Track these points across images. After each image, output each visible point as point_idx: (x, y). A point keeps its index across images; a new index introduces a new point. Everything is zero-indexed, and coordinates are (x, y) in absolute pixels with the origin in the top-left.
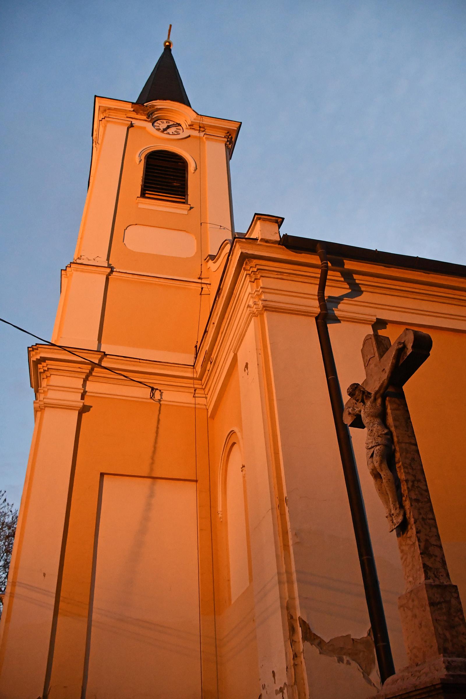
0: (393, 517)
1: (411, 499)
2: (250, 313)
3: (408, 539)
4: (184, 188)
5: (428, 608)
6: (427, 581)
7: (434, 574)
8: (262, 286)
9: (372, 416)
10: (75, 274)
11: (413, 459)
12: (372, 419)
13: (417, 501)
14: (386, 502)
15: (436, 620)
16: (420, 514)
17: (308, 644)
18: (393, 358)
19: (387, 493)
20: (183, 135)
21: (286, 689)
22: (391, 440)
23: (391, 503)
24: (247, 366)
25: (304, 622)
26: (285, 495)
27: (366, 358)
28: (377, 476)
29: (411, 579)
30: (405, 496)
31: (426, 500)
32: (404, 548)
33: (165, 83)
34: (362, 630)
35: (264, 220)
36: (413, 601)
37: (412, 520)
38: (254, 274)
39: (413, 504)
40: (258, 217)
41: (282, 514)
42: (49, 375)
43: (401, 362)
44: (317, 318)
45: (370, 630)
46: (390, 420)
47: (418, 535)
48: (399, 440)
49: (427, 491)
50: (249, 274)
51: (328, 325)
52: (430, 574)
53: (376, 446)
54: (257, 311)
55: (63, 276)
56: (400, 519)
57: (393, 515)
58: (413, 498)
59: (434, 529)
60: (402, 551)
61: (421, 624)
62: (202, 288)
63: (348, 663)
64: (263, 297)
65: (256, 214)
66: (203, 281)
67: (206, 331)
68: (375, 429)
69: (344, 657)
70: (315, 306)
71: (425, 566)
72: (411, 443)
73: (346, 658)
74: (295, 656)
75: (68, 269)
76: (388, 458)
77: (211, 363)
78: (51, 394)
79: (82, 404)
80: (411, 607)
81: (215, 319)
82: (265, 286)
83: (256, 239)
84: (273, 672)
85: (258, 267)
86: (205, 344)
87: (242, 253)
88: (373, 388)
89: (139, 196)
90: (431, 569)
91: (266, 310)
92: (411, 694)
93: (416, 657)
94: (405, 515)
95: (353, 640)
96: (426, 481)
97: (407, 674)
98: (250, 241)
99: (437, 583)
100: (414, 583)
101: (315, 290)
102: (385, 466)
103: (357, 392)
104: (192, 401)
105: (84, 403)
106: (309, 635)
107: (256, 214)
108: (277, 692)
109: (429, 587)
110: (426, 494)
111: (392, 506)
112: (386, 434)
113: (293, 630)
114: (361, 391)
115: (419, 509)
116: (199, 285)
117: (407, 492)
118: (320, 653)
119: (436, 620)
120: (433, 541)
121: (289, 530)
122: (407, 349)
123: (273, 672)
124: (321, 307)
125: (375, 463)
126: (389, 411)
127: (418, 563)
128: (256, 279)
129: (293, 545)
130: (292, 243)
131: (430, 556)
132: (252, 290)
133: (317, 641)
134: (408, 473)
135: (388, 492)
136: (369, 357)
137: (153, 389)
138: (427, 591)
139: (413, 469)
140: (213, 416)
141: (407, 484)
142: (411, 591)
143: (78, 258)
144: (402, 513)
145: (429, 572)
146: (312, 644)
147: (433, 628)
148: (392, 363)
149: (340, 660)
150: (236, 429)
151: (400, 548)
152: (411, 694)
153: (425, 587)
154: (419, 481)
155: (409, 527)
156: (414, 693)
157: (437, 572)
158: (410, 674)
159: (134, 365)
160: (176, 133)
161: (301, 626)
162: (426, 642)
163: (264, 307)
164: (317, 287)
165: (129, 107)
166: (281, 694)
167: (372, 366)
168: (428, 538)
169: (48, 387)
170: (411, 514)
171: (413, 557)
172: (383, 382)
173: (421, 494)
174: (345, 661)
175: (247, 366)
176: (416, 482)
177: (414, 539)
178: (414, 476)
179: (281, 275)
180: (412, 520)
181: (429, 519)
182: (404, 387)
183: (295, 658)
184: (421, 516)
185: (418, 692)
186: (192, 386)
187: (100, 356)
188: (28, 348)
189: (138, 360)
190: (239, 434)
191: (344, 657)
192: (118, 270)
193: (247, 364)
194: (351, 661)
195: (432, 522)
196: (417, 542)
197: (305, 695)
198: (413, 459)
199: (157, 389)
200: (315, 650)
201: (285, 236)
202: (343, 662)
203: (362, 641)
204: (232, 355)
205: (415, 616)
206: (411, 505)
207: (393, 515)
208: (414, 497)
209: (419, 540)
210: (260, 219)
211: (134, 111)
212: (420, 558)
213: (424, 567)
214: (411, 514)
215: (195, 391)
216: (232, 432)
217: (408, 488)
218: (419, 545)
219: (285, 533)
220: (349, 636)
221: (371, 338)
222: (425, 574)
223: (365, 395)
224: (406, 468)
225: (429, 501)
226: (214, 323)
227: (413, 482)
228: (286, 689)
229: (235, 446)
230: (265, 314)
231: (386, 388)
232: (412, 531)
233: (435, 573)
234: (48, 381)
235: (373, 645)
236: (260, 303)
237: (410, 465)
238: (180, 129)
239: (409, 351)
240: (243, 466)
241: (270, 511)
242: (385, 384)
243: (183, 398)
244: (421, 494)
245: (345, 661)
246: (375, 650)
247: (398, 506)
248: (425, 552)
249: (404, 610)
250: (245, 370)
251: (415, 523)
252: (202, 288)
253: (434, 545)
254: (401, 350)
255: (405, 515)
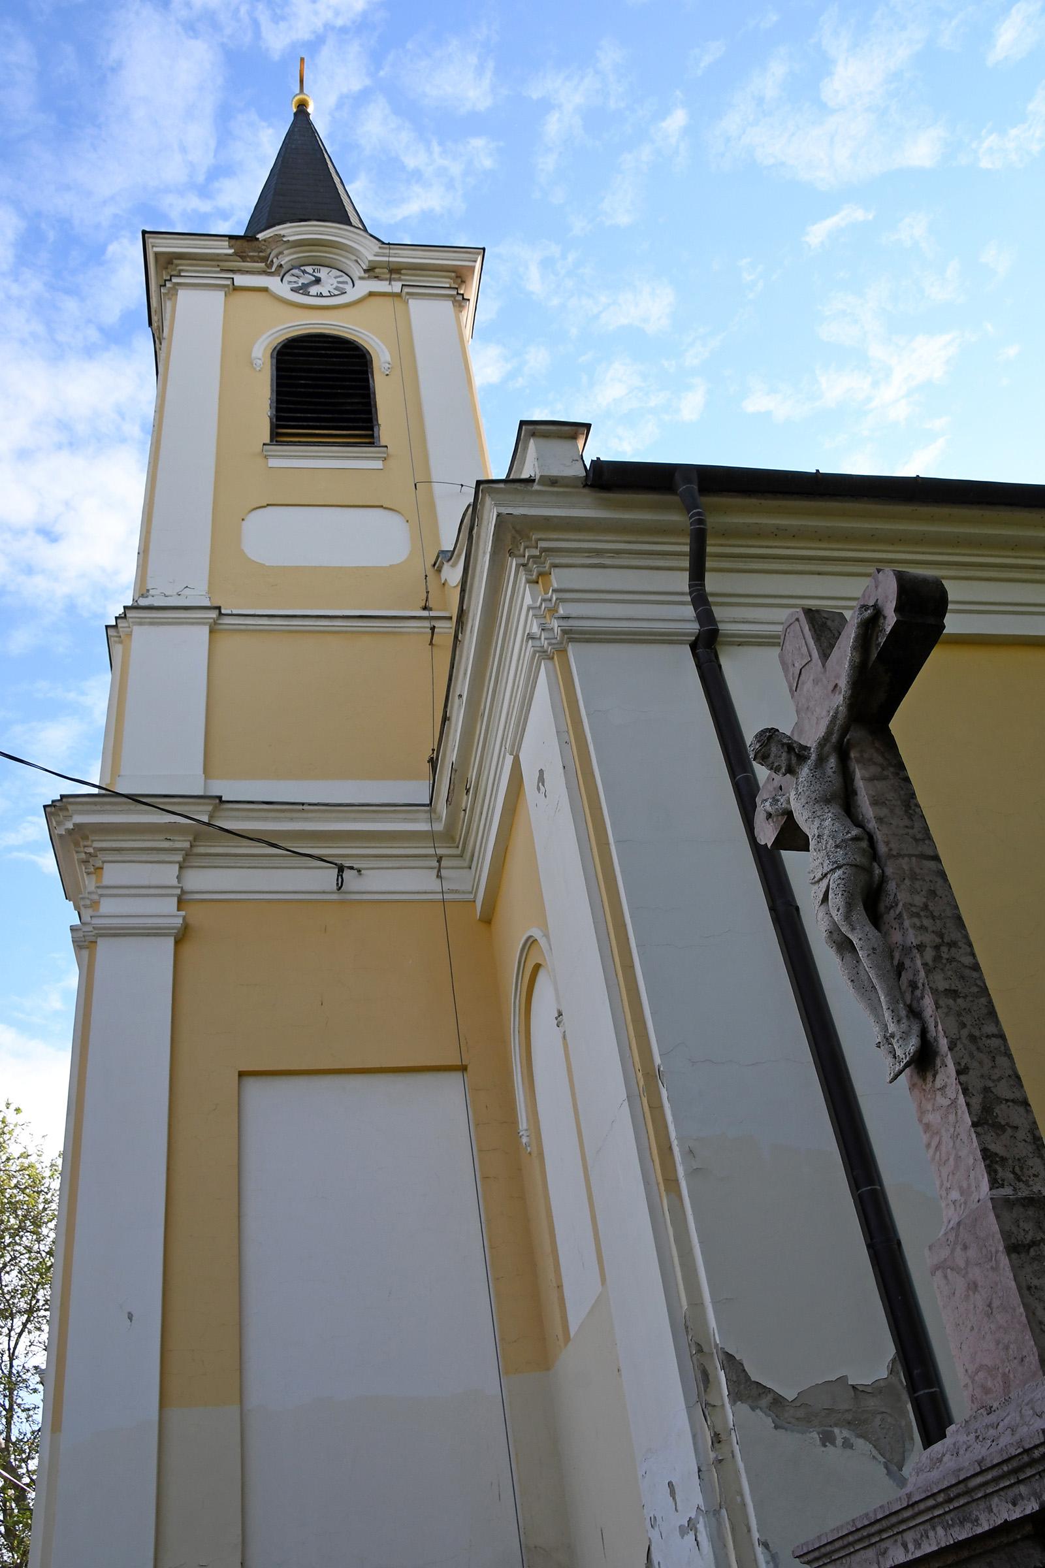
0: (894, 1041)
1: (934, 991)
2: (535, 652)
3: (939, 1093)
4: (370, 412)
5: (1004, 1261)
6: (994, 1192)
7: (1013, 1172)
8: (555, 586)
9: (817, 801)
10: (136, 629)
11: (933, 893)
12: (817, 807)
13: (953, 993)
14: (875, 1009)
15: (1029, 1288)
16: (963, 1025)
17: (743, 1408)
18: (854, 648)
19: (873, 987)
20: (353, 294)
21: (701, 1520)
22: (874, 855)
23: (885, 1007)
24: (541, 779)
25: (729, 1357)
26: (658, 1060)
27: (791, 669)
28: (844, 946)
29: (955, 1195)
30: (920, 985)
31: (975, 989)
32: (931, 1118)
33: (304, 184)
34: (874, 1359)
35: (546, 436)
36: (965, 1248)
37: (943, 1044)
38: (535, 563)
39: (941, 1003)
40: (529, 429)
41: (656, 1108)
42: (99, 864)
43: (874, 655)
44: (694, 646)
45: (894, 1361)
46: (867, 810)
47: (963, 1078)
48: (891, 850)
49: (976, 967)
50: (524, 565)
51: (725, 662)
52: (1003, 1173)
53: (833, 870)
54: (549, 644)
55: (112, 640)
56: (913, 1044)
57: (893, 1036)
58: (941, 988)
59: (1002, 1060)
60: (927, 1127)
61: (989, 1306)
62: (433, 629)
63: (847, 1444)
64: (561, 612)
65: (522, 423)
66: (432, 614)
67: (445, 719)
68: (826, 832)
69: (836, 1431)
70: (685, 618)
71: (987, 1154)
72: (923, 856)
73: (840, 1433)
74: (717, 1439)
75: (121, 623)
76: (870, 898)
77: (468, 791)
78: (108, 906)
79: (180, 921)
80: (962, 1264)
81: (463, 686)
82: (563, 586)
83: (530, 481)
84: (670, 1484)
85: (542, 544)
86: (448, 752)
87: (499, 515)
88: (811, 736)
89: (268, 441)
90: (1003, 1159)
91: (571, 640)
92: (973, 1483)
93: (987, 1391)
94: (924, 1033)
95: (853, 1387)
96: (970, 945)
97: (965, 1438)
98: (517, 486)
99: (1024, 1192)
100: (965, 1203)
101: (681, 582)
102: (860, 914)
103: (774, 749)
104: (435, 885)
105: (184, 918)
106: (746, 1389)
107: (522, 423)
108: (683, 1531)
109: (1001, 1206)
110: (975, 975)
111: (887, 1015)
112: (856, 839)
113: (706, 1378)
114: (783, 745)
115: (959, 1015)
116: (427, 624)
117: (922, 974)
118: (776, 1427)
119: (1029, 1288)
120: (1003, 1090)
121: (675, 1143)
122: (885, 618)
123: (670, 1484)
124: (699, 618)
125: (834, 913)
126: (860, 784)
127: (970, 1148)
128: (540, 574)
129: (687, 1175)
130: (611, 478)
131: (999, 1128)
132: (534, 599)
133: (765, 1401)
134: (923, 928)
135: (874, 981)
136: (798, 666)
137: (341, 869)
138: (997, 1217)
139: (933, 918)
140: (487, 919)
141: (922, 956)
142: (959, 1223)
143: (142, 596)
144: (916, 1029)
145: (999, 1169)
146: (753, 1409)
147: (1022, 1310)
148: (851, 661)
149: (827, 1439)
150: (536, 933)
151: (920, 1121)
152: (973, 1483)
153: (990, 1205)
154: (952, 944)
155: (938, 1062)
156: (979, 1480)
157: (1022, 1168)
158: (973, 1436)
159: (292, 819)
160: (337, 292)
161: (723, 1368)
162: (1007, 1348)
163: (564, 632)
164: (686, 575)
165: (225, 249)
166: (692, 1533)
167: (808, 686)
168: (991, 1084)
169: (100, 891)
170: (940, 1027)
171: (955, 1137)
172: (837, 712)
173: (962, 977)
174: (839, 1441)
175: (541, 779)
176: (944, 949)
177: (953, 1090)
178: (941, 936)
179: (598, 559)
180: (943, 1044)
181: (988, 1037)
182: (891, 725)
183: (716, 1445)
184: (965, 1033)
185: (989, 1476)
186: (432, 851)
187: (210, 808)
188: (45, 807)
189: (301, 807)
190: (542, 942)
191: (836, 1431)
192: (229, 612)
193: (541, 772)
194: (853, 1440)
195: (995, 1042)
196: (961, 1097)
197: (749, 1531)
198: (933, 893)
199: (352, 868)
200: (762, 1421)
201: (597, 463)
202: (833, 1443)
203: (876, 1390)
204: (509, 760)
205: (973, 1287)
206: (938, 1007)
207: (893, 1036)
208: (942, 985)
209: (965, 1091)
210: (533, 435)
211: (235, 254)
212: (974, 1136)
213: (984, 1159)
214: (940, 1027)
215: (439, 861)
216: (531, 942)
217: (925, 965)
218: (968, 1104)
219: (666, 1151)
220: (843, 1379)
221: (797, 620)
222: (989, 1173)
223: (795, 754)
224: (918, 915)
225: (984, 991)
226: (460, 696)
227: (937, 948)
228: (701, 1520)
229: (542, 979)
230: (571, 649)
231: (845, 730)
232: (947, 1073)
233: (1017, 1169)
234: (99, 878)
235: (905, 1396)
236: (555, 624)
237: (926, 907)
238: (346, 283)
239: (891, 619)
240: (560, 1014)
241: (626, 1104)
242: (841, 716)
243: (416, 881)
244: (962, 977)
245: (839, 1441)
246: (909, 1406)
247: (903, 1013)
248: (984, 1121)
249: (946, 1277)
250: (539, 789)
251: (950, 1049)
252: (433, 629)
253: (1007, 1101)
254: (871, 622)
255: (924, 1033)
